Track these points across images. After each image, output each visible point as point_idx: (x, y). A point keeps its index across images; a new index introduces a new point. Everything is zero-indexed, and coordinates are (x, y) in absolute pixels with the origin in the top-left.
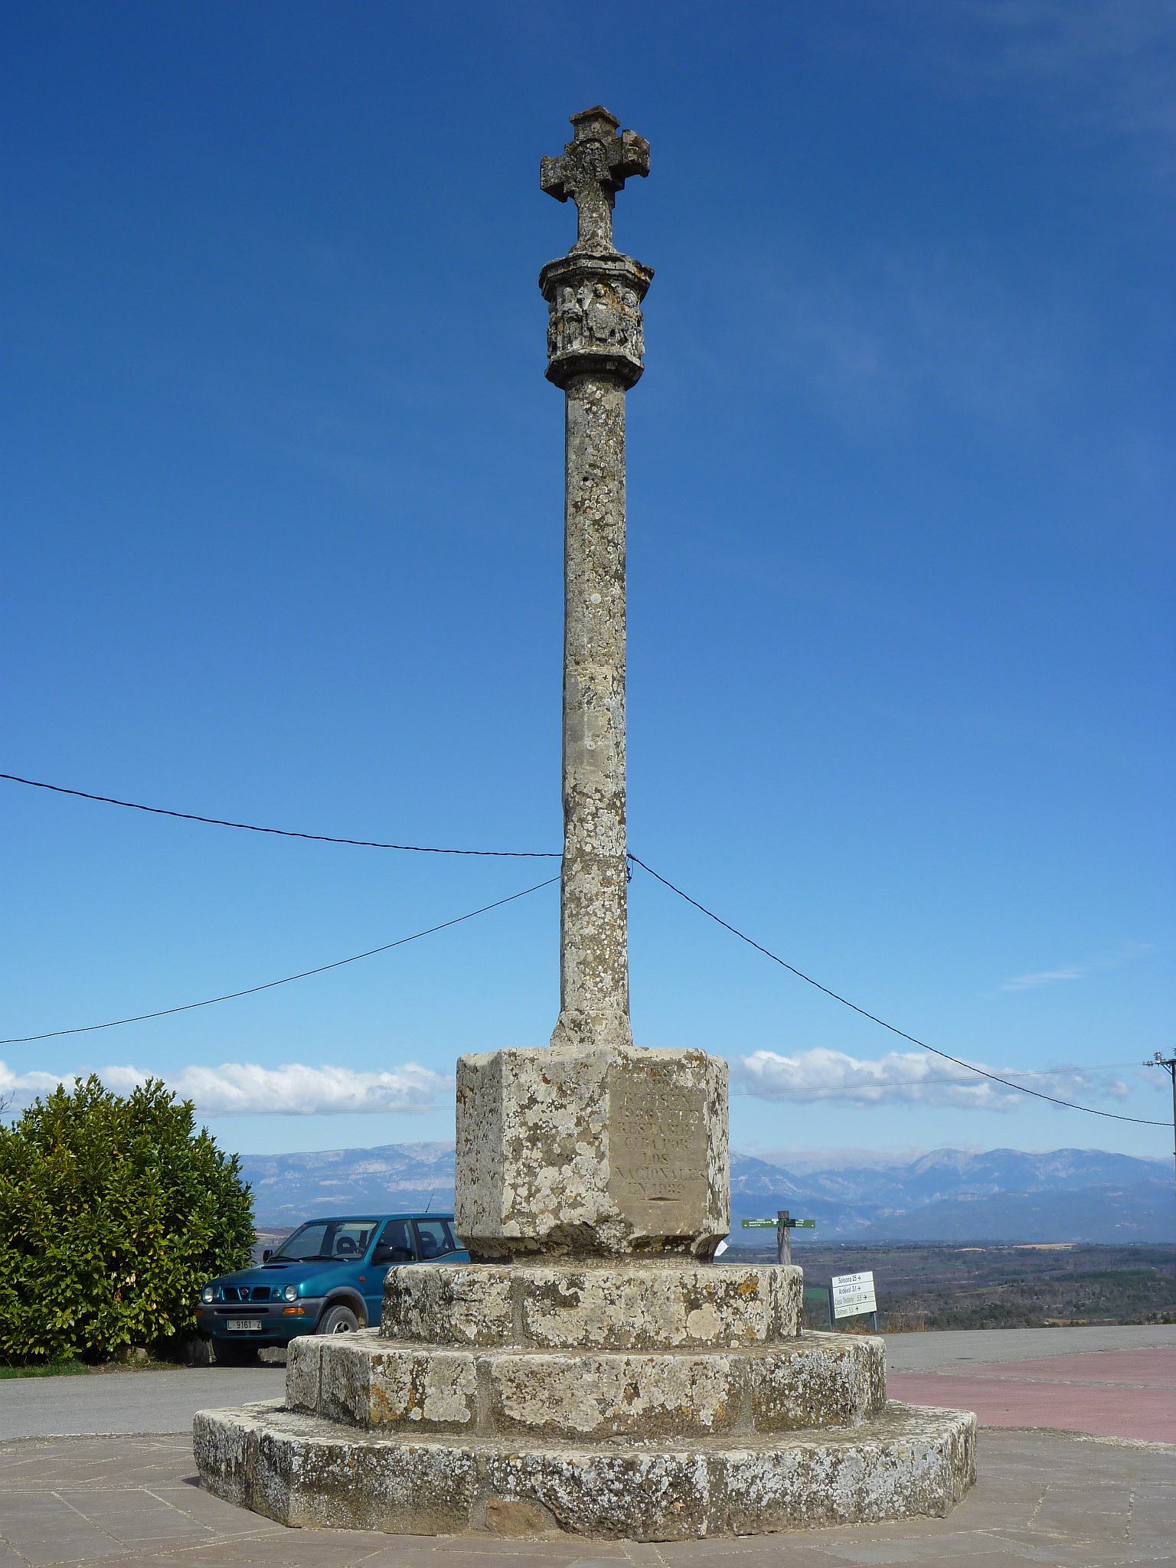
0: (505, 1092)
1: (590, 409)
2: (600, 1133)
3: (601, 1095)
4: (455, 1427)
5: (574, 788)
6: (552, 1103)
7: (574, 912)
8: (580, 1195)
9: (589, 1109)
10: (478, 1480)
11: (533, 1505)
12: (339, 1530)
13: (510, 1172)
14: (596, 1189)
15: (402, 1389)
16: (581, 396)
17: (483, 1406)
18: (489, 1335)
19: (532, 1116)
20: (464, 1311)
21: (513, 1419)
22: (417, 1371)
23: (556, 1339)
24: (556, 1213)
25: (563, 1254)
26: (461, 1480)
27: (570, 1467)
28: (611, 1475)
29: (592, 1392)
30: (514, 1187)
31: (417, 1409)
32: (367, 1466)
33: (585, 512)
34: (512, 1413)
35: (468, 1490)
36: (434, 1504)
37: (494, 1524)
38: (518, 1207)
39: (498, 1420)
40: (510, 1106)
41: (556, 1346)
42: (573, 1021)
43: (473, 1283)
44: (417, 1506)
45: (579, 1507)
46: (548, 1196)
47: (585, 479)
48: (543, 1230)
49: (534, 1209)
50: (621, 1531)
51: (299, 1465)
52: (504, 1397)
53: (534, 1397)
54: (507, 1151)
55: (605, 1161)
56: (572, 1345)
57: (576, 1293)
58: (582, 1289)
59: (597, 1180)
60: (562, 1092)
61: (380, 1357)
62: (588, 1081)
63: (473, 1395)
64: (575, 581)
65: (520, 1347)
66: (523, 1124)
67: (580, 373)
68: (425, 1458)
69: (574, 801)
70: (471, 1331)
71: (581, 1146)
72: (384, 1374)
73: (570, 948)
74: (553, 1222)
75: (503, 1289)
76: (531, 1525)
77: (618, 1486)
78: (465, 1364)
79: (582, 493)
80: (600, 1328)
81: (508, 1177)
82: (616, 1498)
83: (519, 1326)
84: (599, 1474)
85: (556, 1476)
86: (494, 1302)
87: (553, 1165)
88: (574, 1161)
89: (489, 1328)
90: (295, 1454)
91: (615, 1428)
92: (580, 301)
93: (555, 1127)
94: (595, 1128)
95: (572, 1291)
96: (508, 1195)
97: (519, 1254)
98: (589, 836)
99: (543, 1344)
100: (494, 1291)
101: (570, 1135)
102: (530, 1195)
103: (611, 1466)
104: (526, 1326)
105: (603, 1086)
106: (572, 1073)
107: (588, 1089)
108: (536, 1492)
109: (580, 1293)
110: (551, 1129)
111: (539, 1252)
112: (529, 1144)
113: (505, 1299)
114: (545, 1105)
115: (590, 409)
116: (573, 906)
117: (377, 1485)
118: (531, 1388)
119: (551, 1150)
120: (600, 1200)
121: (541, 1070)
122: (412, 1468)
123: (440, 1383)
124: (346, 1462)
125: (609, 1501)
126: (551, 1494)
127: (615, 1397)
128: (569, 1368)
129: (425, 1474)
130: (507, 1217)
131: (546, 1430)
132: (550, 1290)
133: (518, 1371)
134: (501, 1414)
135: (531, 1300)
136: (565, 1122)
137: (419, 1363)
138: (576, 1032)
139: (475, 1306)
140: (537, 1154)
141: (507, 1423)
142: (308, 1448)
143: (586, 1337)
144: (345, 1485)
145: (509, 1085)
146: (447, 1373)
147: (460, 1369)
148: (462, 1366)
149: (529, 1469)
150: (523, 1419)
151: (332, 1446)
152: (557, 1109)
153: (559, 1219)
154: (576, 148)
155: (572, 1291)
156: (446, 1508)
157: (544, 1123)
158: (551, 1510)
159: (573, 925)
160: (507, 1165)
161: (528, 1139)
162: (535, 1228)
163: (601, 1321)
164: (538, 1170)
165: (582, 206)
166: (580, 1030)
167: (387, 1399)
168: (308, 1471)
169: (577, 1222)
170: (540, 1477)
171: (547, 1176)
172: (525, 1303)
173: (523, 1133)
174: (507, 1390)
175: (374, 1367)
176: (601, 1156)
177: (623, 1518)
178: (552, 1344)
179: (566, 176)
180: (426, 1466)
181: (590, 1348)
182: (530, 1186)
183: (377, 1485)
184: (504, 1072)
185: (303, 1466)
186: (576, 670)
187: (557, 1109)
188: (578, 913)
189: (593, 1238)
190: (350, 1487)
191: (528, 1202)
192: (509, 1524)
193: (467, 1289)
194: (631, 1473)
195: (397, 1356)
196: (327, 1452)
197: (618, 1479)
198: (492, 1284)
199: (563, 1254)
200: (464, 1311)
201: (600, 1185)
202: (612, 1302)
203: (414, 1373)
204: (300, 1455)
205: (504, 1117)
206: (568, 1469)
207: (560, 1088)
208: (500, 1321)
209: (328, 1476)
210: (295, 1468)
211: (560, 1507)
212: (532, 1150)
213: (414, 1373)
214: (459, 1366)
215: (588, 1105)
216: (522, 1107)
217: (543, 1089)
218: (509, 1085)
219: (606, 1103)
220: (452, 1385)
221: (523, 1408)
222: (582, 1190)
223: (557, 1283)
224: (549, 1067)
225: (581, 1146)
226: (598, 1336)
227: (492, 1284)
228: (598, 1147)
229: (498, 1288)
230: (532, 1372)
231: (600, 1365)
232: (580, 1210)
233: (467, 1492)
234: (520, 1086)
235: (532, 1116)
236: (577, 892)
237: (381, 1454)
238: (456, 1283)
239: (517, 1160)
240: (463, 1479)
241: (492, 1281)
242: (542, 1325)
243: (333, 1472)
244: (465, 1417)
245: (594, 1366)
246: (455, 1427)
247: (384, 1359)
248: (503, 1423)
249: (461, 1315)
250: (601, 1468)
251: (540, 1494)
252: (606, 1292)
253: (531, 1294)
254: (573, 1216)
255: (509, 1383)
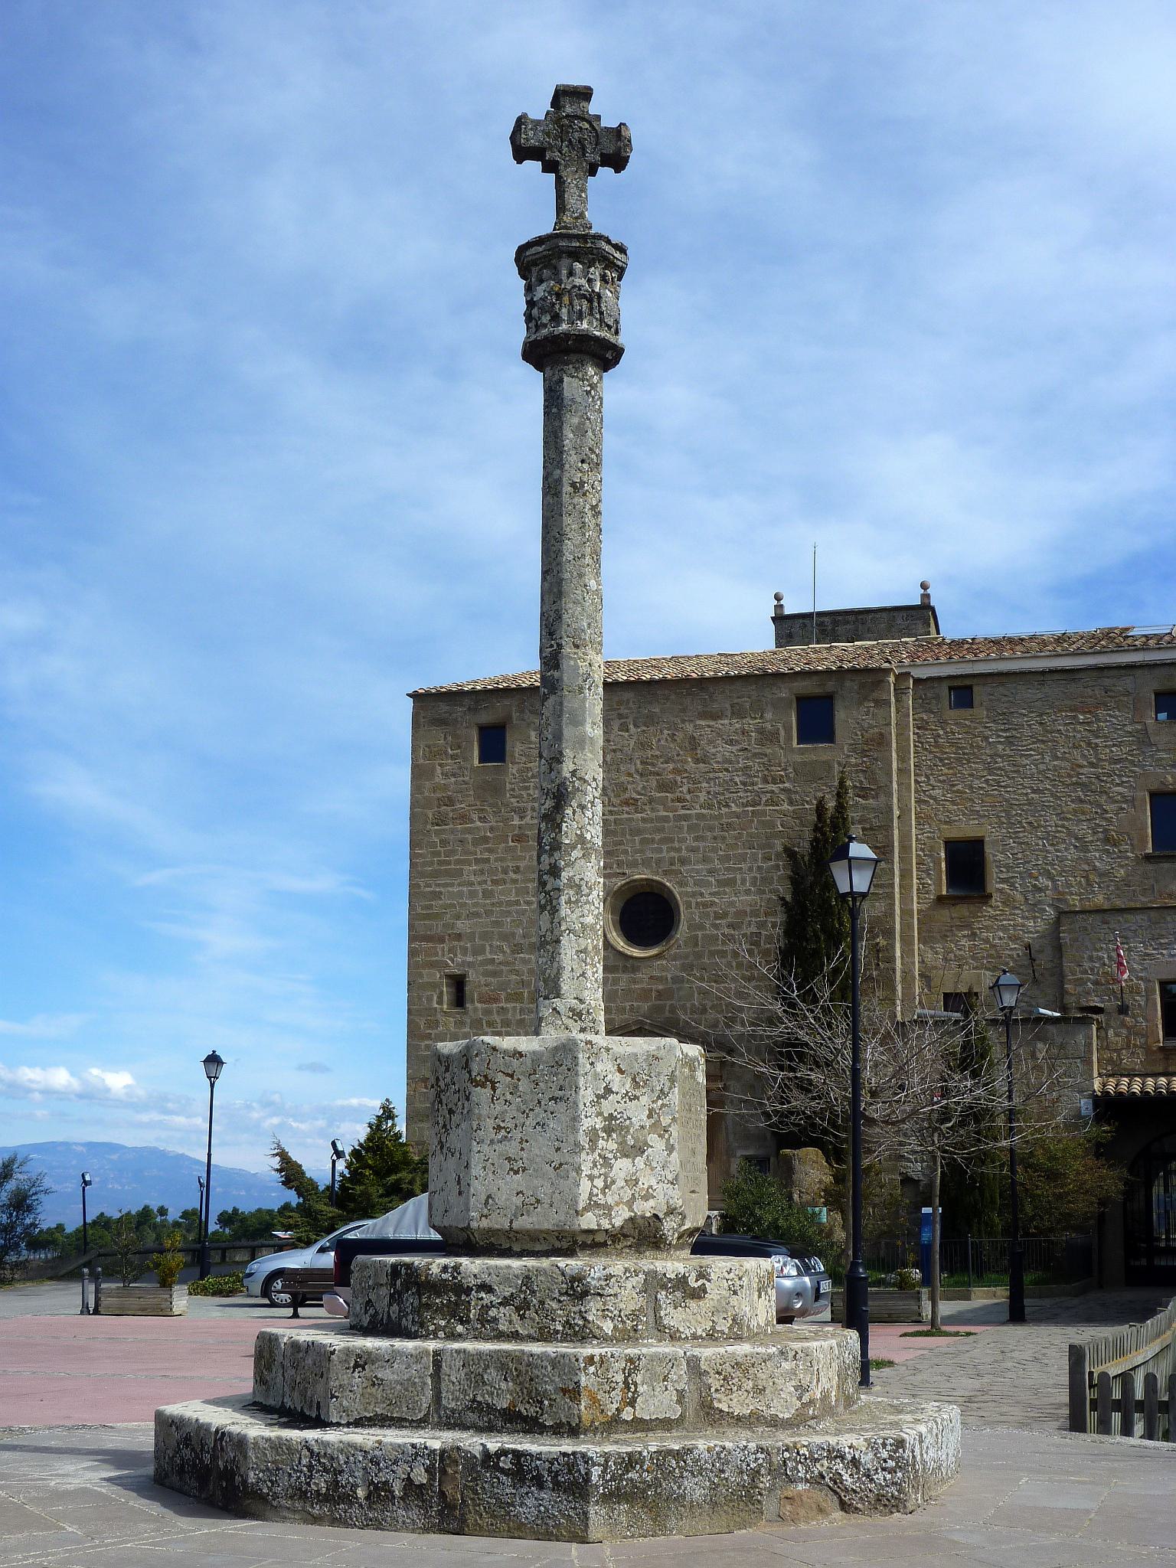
0: (581, 1081)
1: (590, 391)
2: (670, 1126)
3: (670, 1088)
4: (666, 1424)
5: (574, 773)
6: (627, 1094)
7: (573, 899)
8: (651, 1187)
9: (660, 1102)
10: (770, 1472)
11: (821, 1490)
12: (640, 1539)
13: (586, 1161)
14: (666, 1182)
15: (614, 1389)
16: (580, 375)
17: (693, 1400)
18: (625, 1330)
19: (608, 1106)
20: (600, 1305)
21: (721, 1411)
22: (630, 1369)
23: (687, 1331)
24: (630, 1204)
25: (626, 1247)
26: (755, 1474)
27: (852, 1451)
28: (885, 1455)
29: (791, 1379)
30: (591, 1178)
31: (629, 1409)
32: (666, 1469)
33: (584, 494)
34: (720, 1406)
35: (762, 1482)
36: (731, 1501)
37: (788, 1514)
38: (594, 1199)
39: (708, 1414)
40: (586, 1095)
41: (687, 1337)
42: (572, 1010)
43: (609, 1277)
44: (714, 1504)
45: (860, 1487)
46: (623, 1187)
47: (583, 461)
48: (618, 1222)
49: (610, 1201)
50: (893, 1506)
51: (599, 1475)
52: (713, 1390)
53: (740, 1388)
54: (584, 1140)
55: (675, 1154)
56: (701, 1337)
57: (704, 1284)
58: (709, 1281)
59: (667, 1172)
60: (636, 1084)
61: (592, 1357)
62: (659, 1074)
63: (683, 1390)
64: (573, 562)
65: (653, 1340)
66: (600, 1114)
67: (587, 353)
68: (722, 1456)
69: (573, 786)
70: (608, 1327)
71: (652, 1139)
72: (596, 1374)
73: (568, 935)
74: (627, 1214)
75: (638, 1282)
76: (821, 1510)
77: (891, 1464)
78: (676, 1359)
79: (580, 475)
80: (725, 1318)
81: (586, 1170)
82: (890, 1476)
83: (652, 1320)
84: (875, 1455)
85: (838, 1460)
86: (628, 1297)
87: (627, 1156)
88: (646, 1153)
89: (623, 1322)
90: (594, 1464)
91: (811, 1412)
92: (590, 281)
93: (629, 1118)
94: (665, 1120)
95: (700, 1283)
96: (585, 1186)
97: (584, 1246)
98: (589, 824)
99: (674, 1337)
100: (629, 1285)
101: (642, 1127)
102: (606, 1187)
103: (884, 1445)
104: (658, 1320)
105: (672, 1079)
106: (644, 1064)
107: (659, 1081)
108: (823, 1477)
109: (708, 1284)
110: (625, 1120)
111: (604, 1244)
112: (604, 1134)
113: (640, 1293)
114: (619, 1096)
115: (590, 391)
116: (572, 892)
117: (675, 1488)
118: (737, 1380)
119: (625, 1142)
120: (670, 1192)
121: (616, 1060)
122: (709, 1467)
123: (650, 1382)
124: (645, 1467)
125: (885, 1479)
126: (837, 1479)
127: (810, 1383)
128: (770, 1357)
129: (723, 1471)
130: (584, 1209)
131: (751, 1421)
132: (681, 1282)
133: (725, 1363)
134: (711, 1407)
135: (664, 1293)
136: (637, 1114)
137: (630, 1360)
138: (576, 1021)
139: (610, 1300)
140: (612, 1146)
141: (717, 1416)
142: (607, 1456)
143: (713, 1328)
144: (644, 1491)
145: (586, 1074)
146: (658, 1369)
147: (670, 1364)
148: (672, 1361)
149: (816, 1456)
150: (731, 1410)
151: (632, 1452)
152: (631, 1100)
153: (633, 1211)
154: (561, 119)
155: (700, 1283)
156: (741, 1503)
157: (618, 1113)
158: (836, 1493)
159: (572, 912)
160: (583, 1155)
161: (604, 1130)
162: (610, 1220)
163: (726, 1312)
164: (613, 1161)
165: (569, 181)
166: (581, 1019)
167: (599, 1400)
168: (607, 1481)
169: (648, 1215)
170: (826, 1463)
171: (622, 1167)
172: (659, 1296)
173: (599, 1124)
174: (715, 1382)
175: (585, 1368)
176: (670, 1149)
177: (897, 1493)
178: (683, 1336)
179: (549, 143)
180: (723, 1464)
181: (716, 1339)
182: (606, 1178)
183: (675, 1488)
184: (581, 1061)
185: (602, 1476)
186: (575, 653)
187: (631, 1100)
188: (577, 901)
189: (658, 1229)
190: (649, 1493)
191: (604, 1194)
192: (802, 1512)
193: (604, 1283)
194: (901, 1450)
195: (609, 1355)
196: (627, 1459)
197: (891, 1458)
198: (627, 1278)
199: (626, 1247)
200: (600, 1305)
201: (670, 1177)
202: (735, 1293)
203: (627, 1371)
204: (599, 1465)
205: (581, 1106)
206: (849, 1453)
207: (634, 1079)
208: (635, 1315)
209: (627, 1484)
210: (594, 1479)
211: (846, 1490)
212: (607, 1141)
213: (627, 1371)
214: (670, 1361)
215: (659, 1098)
216: (599, 1097)
217: (618, 1079)
218: (586, 1074)
219: (675, 1097)
220: (664, 1381)
221: (731, 1400)
222: (653, 1182)
223: (687, 1275)
224: (623, 1057)
225: (652, 1139)
226: (723, 1326)
227: (627, 1278)
228: (668, 1140)
229: (634, 1281)
230: (737, 1364)
231: (797, 1353)
232: (651, 1203)
233: (761, 1485)
234: (596, 1075)
235: (608, 1106)
236: (577, 879)
237: (678, 1455)
238: (593, 1278)
239: (593, 1151)
240: (758, 1472)
241: (628, 1275)
242: (674, 1317)
243: (632, 1480)
244: (675, 1413)
245: (791, 1354)
246: (666, 1424)
247: (597, 1359)
248: (711, 1415)
249: (598, 1310)
250: (877, 1449)
251: (827, 1479)
252: (730, 1283)
253: (664, 1287)
254: (645, 1208)
255: (717, 1376)
